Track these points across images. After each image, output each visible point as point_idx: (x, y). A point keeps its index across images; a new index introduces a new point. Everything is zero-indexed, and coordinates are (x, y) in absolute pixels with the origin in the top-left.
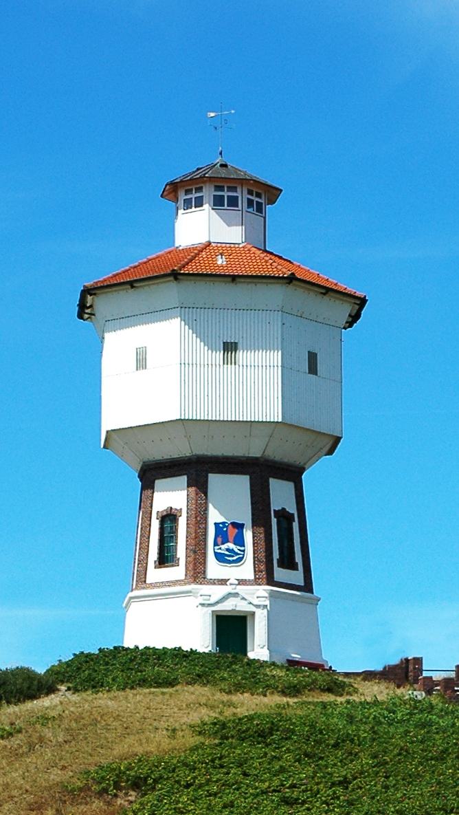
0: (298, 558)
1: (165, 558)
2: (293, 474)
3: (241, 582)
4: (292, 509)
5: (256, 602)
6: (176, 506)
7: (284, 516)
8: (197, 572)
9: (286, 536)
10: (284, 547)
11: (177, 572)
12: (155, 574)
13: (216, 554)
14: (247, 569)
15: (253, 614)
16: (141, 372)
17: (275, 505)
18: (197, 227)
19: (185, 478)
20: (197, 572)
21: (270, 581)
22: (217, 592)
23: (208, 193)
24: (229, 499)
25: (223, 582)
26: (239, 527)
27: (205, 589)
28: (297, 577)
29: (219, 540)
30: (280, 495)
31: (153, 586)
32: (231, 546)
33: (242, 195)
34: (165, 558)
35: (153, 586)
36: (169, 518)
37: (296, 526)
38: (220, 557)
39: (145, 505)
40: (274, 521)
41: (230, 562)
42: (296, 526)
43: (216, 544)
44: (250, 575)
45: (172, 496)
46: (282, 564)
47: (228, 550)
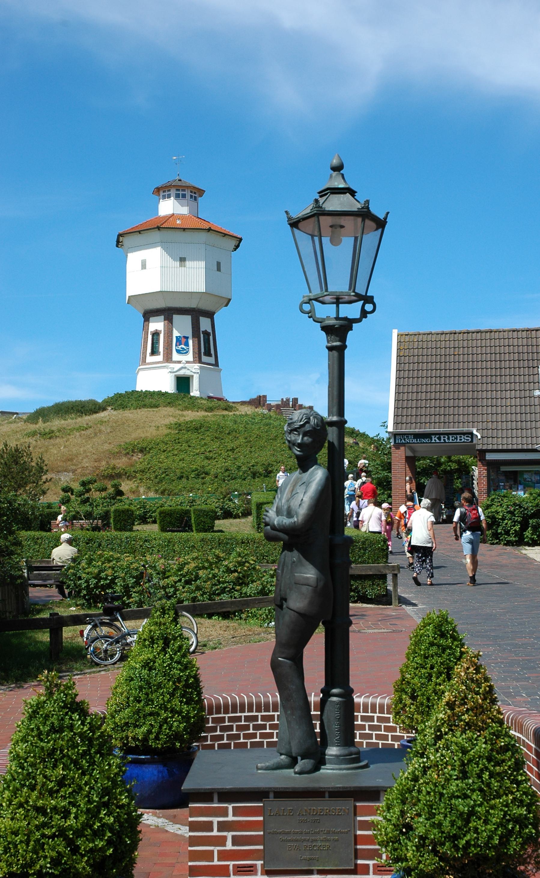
0: (212, 352)
1: (154, 352)
2: (210, 315)
3: (188, 362)
4: (210, 330)
5: (194, 371)
6: (159, 329)
7: (206, 333)
8: (168, 358)
9: (207, 342)
10: (206, 347)
11: (159, 358)
12: (150, 359)
13: (176, 350)
14: (190, 357)
15: (193, 376)
16: (144, 270)
17: (202, 329)
18: (168, 207)
19: (163, 316)
20: (168, 358)
21: (200, 362)
22: (177, 366)
23: (173, 192)
24: (182, 326)
25: (179, 362)
26: (187, 338)
27: (172, 365)
28: (212, 360)
29: (178, 344)
30: (205, 324)
31: (149, 364)
32: (183, 346)
33: (188, 193)
34: (154, 352)
35: (149, 364)
36: (156, 334)
37: (211, 337)
38: (178, 351)
39: (145, 328)
40: (202, 335)
41: (182, 353)
42: (211, 337)
43: (176, 345)
44: (192, 359)
45: (157, 325)
46: (205, 354)
47: (182, 348)
